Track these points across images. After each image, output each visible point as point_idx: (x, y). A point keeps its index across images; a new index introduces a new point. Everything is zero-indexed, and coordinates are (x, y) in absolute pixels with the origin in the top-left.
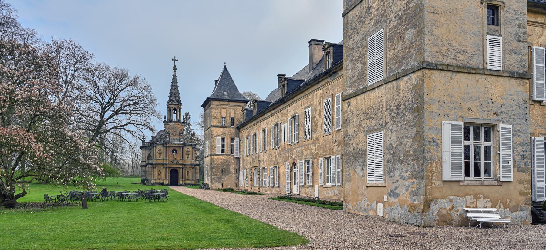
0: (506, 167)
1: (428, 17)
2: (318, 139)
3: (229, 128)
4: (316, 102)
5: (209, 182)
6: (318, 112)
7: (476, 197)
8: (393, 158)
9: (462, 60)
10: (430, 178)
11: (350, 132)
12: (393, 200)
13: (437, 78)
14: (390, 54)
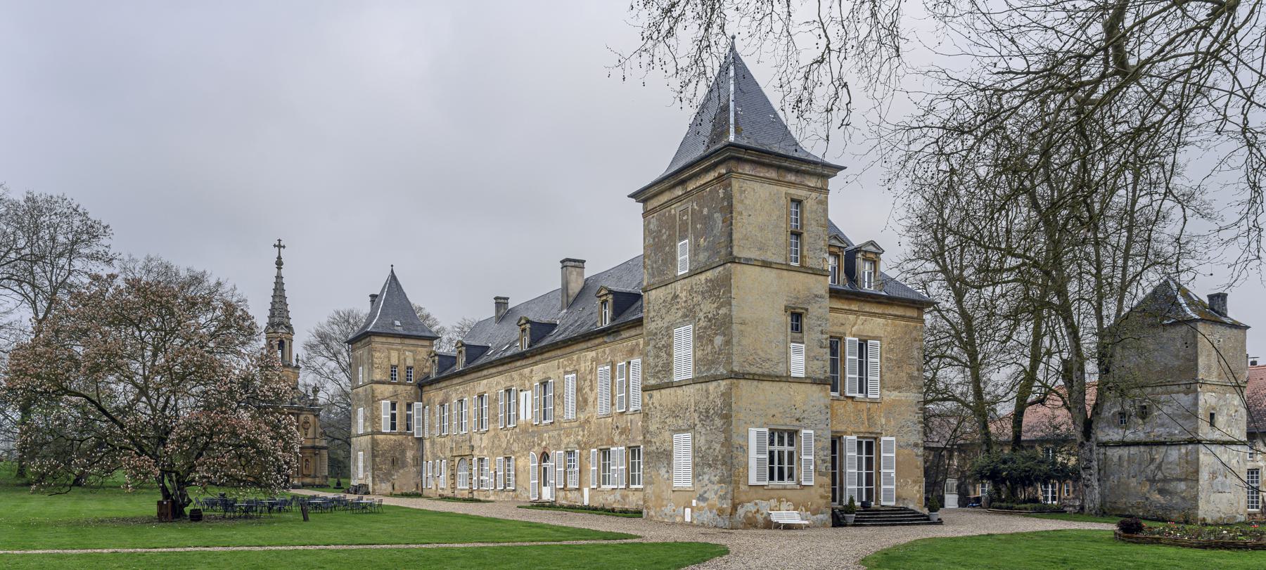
0: (808, 471)
1: (736, 328)
2: (587, 421)
3: (404, 384)
4: (584, 366)
5: (369, 482)
6: (588, 383)
7: (780, 501)
8: (701, 462)
9: (767, 368)
10: (737, 483)
11: (653, 428)
12: (702, 504)
13: (746, 388)
14: (699, 353)
